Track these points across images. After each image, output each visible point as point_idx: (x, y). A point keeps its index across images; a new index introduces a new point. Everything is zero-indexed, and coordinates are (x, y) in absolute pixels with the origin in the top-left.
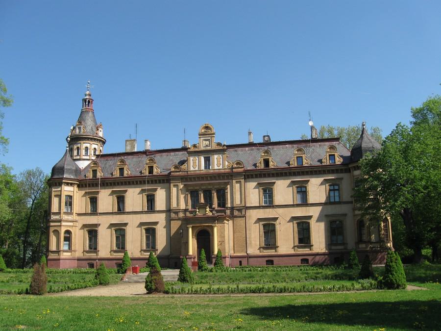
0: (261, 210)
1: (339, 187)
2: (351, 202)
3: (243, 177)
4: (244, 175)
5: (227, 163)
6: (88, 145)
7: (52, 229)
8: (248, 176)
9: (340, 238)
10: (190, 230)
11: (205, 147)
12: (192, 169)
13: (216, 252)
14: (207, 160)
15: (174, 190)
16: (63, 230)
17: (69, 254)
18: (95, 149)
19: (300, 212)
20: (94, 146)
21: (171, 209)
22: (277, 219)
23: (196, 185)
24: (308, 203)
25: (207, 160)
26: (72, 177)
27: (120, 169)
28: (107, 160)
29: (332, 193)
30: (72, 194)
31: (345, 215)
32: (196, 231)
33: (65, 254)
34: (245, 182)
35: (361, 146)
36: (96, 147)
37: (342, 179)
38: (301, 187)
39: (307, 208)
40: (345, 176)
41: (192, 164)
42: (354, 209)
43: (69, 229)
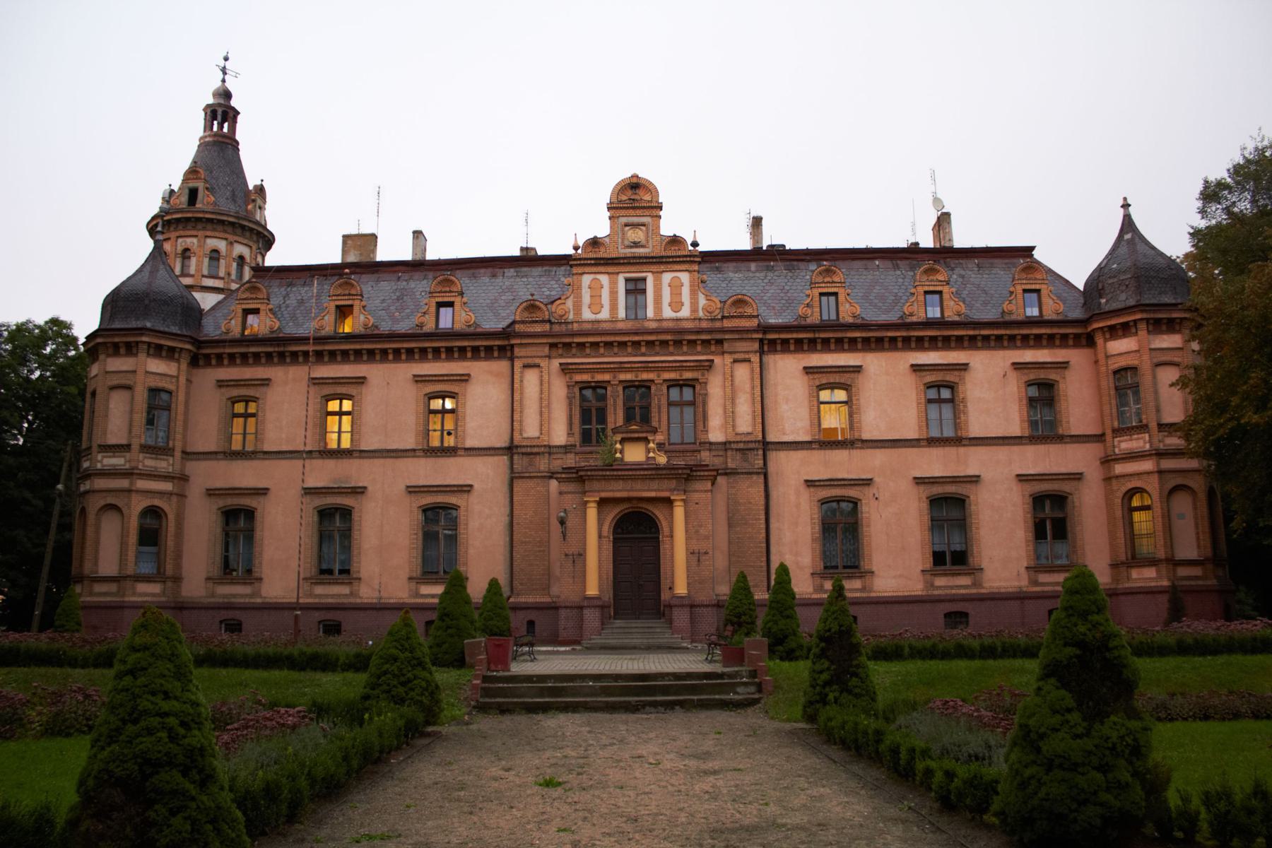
0: (815, 452)
1: (850, 396)
2: (1099, 438)
3: (756, 346)
4: (761, 341)
5: (702, 301)
6: (222, 245)
7: (94, 504)
8: (772, 343)
9: (1061, 548)
10: (592, 513)
11: (631, 247)
12: (587, 315)
13: (681, 589)
14: (636, 289)
15: (531, 380)
16: (138, 505)
17: (155, 588)
18: (241, 258)
19: (936, 463)
20: (239, 249)
21: (516, 443)
22: (868, 482)
23: (646, 367)
24: (1061, 432)
25: (636, 289)
26: (175, 329)
27: (338, 307)
28: (291, 285)
29: (933, 411)
30: (171, 387)
31: (1077, 477)
32: (612, 514)
33: (142, 587)
34: (1106, 340)
35: (550, 349)
36: (246, 252)
37: (1064, 366)
38: (938, 386)
39: (962, 450)
40: (1076, 357)
41: (586, 298)
42: (1107, 461)
43: (157, 502)
